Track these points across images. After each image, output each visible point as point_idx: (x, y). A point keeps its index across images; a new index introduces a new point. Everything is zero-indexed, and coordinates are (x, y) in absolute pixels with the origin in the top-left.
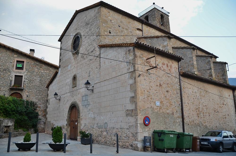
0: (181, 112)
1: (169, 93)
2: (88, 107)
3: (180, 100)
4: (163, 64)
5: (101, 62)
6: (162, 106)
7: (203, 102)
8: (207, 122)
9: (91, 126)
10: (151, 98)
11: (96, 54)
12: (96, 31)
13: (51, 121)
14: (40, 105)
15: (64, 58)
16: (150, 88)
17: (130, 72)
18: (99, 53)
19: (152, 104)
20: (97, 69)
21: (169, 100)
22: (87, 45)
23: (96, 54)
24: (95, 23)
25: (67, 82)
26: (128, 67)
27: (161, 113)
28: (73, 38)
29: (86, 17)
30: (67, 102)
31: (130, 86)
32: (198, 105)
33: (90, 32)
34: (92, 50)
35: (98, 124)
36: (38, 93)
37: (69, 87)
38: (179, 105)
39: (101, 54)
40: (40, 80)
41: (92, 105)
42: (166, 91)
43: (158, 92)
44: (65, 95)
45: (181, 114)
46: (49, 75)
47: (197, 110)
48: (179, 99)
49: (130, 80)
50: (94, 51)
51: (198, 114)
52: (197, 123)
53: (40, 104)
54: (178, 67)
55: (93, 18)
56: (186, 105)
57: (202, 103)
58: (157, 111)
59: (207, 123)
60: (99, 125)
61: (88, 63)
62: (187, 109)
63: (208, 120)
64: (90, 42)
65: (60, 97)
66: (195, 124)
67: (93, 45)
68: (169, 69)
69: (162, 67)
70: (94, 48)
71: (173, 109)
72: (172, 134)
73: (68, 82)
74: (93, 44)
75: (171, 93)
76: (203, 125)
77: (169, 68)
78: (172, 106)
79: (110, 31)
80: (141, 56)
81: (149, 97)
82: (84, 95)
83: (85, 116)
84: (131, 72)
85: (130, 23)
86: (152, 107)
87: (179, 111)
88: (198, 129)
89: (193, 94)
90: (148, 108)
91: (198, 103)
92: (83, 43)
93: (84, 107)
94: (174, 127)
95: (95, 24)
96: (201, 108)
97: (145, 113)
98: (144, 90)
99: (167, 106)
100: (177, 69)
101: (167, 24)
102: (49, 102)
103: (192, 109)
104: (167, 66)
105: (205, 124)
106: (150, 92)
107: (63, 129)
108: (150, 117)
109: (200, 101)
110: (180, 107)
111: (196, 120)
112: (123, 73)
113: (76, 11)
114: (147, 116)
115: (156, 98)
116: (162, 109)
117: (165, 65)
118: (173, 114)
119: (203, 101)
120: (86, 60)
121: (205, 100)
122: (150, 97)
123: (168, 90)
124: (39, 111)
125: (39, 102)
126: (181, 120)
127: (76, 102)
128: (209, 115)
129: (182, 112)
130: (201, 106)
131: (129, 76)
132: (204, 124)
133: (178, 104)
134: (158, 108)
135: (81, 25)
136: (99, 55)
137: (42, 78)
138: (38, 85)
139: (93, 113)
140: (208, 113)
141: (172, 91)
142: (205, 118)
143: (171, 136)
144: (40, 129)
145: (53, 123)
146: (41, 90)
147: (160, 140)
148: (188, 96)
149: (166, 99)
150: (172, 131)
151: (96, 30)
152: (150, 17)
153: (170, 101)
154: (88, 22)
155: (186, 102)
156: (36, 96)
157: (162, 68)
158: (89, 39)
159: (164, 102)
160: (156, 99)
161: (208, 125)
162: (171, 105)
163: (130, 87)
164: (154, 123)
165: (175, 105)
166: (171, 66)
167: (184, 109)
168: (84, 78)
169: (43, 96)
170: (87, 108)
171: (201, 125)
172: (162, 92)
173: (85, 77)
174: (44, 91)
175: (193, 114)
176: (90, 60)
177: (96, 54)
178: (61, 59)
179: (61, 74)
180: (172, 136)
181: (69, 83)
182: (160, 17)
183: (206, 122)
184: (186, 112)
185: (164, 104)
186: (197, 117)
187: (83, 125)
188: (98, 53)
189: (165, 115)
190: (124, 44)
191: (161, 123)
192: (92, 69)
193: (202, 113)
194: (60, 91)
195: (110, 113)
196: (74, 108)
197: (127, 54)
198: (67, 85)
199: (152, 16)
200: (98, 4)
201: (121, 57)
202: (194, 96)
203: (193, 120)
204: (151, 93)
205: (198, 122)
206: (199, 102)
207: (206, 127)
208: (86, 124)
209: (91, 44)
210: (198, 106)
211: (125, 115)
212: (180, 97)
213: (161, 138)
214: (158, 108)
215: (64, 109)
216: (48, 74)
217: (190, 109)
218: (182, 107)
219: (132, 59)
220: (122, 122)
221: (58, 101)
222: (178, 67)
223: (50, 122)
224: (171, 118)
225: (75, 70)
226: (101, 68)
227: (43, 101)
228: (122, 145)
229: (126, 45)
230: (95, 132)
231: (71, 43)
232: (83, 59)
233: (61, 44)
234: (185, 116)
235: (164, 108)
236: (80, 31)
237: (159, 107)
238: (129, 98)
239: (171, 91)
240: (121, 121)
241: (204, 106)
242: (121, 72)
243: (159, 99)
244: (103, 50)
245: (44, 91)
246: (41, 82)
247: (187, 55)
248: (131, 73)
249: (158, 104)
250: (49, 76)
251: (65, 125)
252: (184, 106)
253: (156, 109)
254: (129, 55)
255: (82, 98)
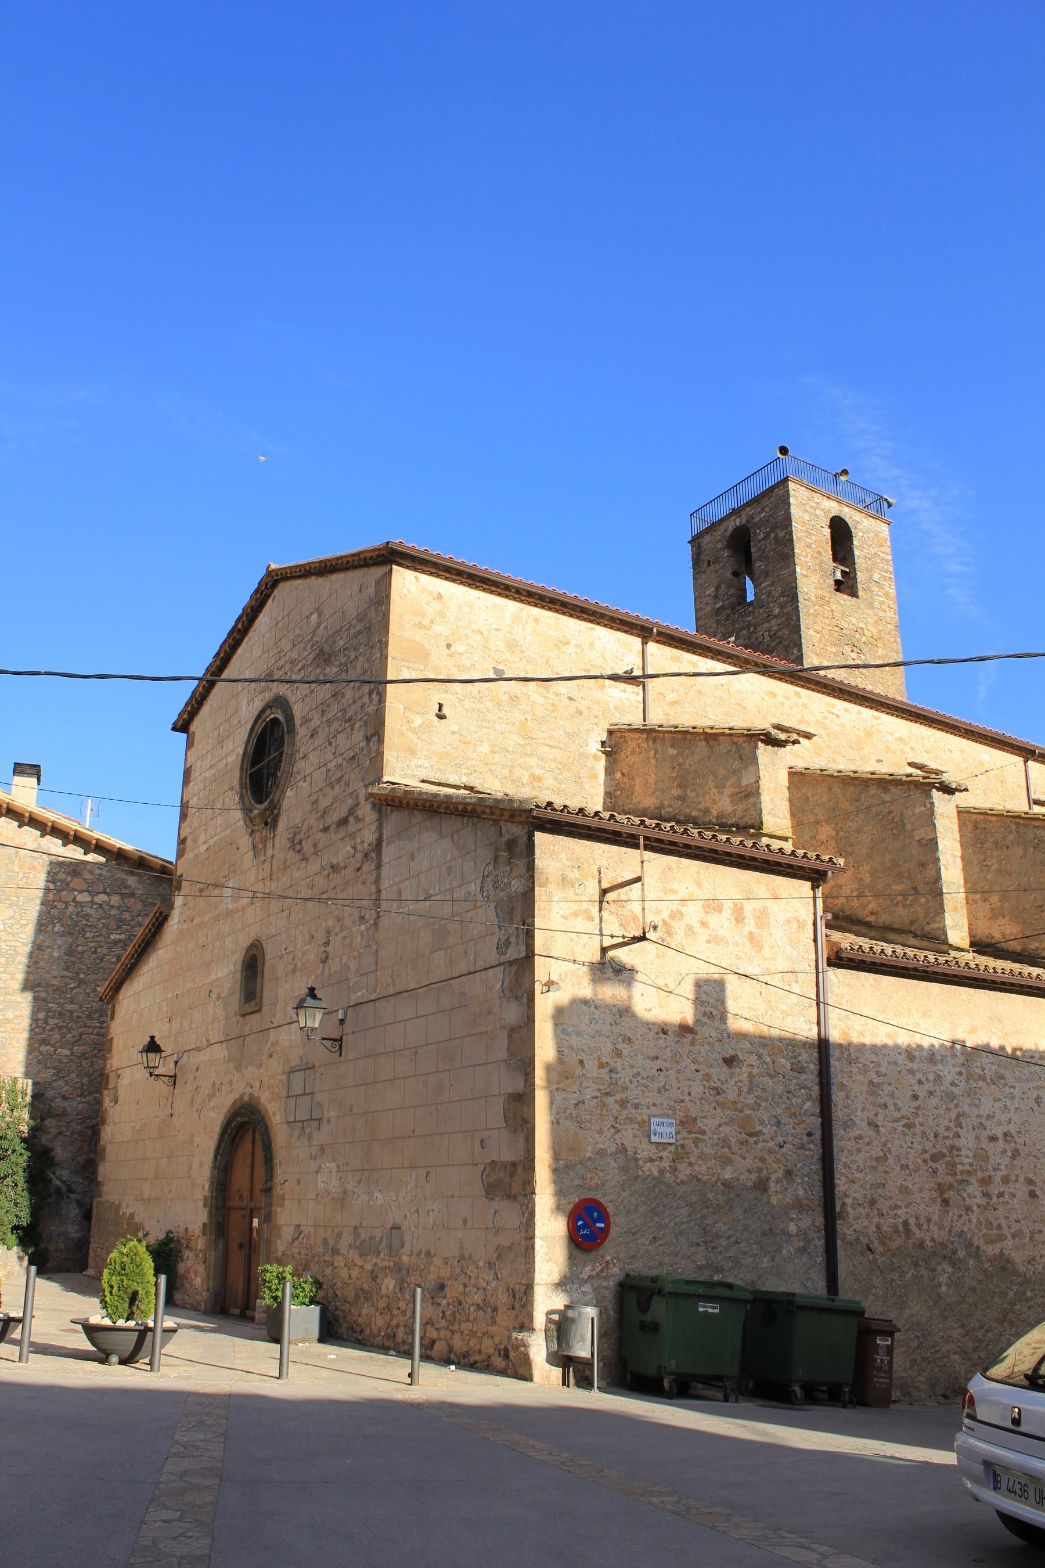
0: (817, 1178)
1: (744, 1069)
2: (315, 1135)
3: (812, 1107)
4: (712, 904)
5: (382, 887)
6: (689, 1143)
7: (989, 1117)
8: (1014, 1236)
9: (325, 1241)
10: (623, 1103)
11: (359, 840)
12: (362, 707)
13: (124, 1205)
14: (66, 1104)
15: (202, 839)
16: (620, 1046)
17: (511, 963)
18: (376, 836)
19: (628, 1136)
20: (363, 927)
21: (736, 1109)
22: (319, 776)
23: (359, 840)
24: (361, 659)
25: (213, 977)
26: (501, 935)
27: (683, 1182)
28: (252, 729)
29: (320, 615)
30: (210, 1097)
31: (510, 1037)
32: (943, 1133)
33: (335, 708)
34: (343, 815)
35: (360, 1231)
36: (52, 1030)
37: (225, 1009)
38: (809, 1135)
39: (384, 843)
40: (70, 952)
41: (333, 1123)
42: (719, 1057)
43: (667, 1065)
44: (202, 1057)
45: (818, 1190)
46: (121, 920)
47: (941, 1166)
48: (809, 1104)
49: (508, 1002)
50: (351, 819)
51: (941, 1188)
52: (933, 1240)
53: (64, 1098)
54: (812, 917)
55: (353, 631)
56: (860, 1137)
57: (975, 1121)
58: (656, 1173)
59: (1009, 1243)
60: (364, 1235)
61: (321, 882)
62: (860, 1159)
63: (1018, 1221)
64: (334, 763)
65: (176, 1062)
66: (921, 1244)
67: (347, 784)
68: (751, 934)
69: (703, 924)
70: (350, 802)
71: (762, 1160)
72: (710, 1299)
73: (218, 979)
74: (346, 777)
75: (755, 1071)
76: (977, 1253)
77: (751, 925)
78: (760, 1145)
79: (440, 710)
80: (574, 874)
81: (607, 1094)
82: (295, 1062)
83: (299, 1182)
84: (515, 961)
85: (568, 643)
86: (623, 1150)
87: (806, 1170)
88: (943, 1279)
89: (911, 1072)
90: (601, 1153)
91: (946, 1123)
92: (303, 764)
93: (296, 1133)
94: (766, 1262)
95: (359, 665)
96: (971, 1154)
97: (577, 1182)
98: (582, 1056)
99: (725, 1143)
100: (801, 926)
101: (876, 577)
102: (116, 1088)
103: (898, 1158)
104: (739, 918)
105: (999, 1245)
106: (619, 1069)
107: (187, 1253)
108: (611, 1202)
109: (966, 1108)
110: (815, 1149)
111: (929, 1220)
112: (481, 964)
113: (269, 573)
114: (601, 1204)
115: (651, 1100)
116: (693, 1159)
117: (721, 912)
118: (762, 1186)
119: (986, 1108)
120: (314, 867)
121: (999, 1104)
122: (618, 1097)
123: (731, 1052)
124: (61, 1138)
125: (61, 1082)
126: (820, 1221)
127: (258, 1099)
128: (1033, 1195)
129: (824, 1176)
130: (967, 1141)
131: (506, 983)
132: (992, 1250)
133: (801, 1130)
134: (664, 1154)
135: (294, 655)
136: (376, 845)
137: (81, 941)
138: (54, 982)
139: (338, 1166)
140: (1021, 1179)
141: (760, 1057)
142: (995, 1209)
143: (701, 1309)
144: (56, 1250)
145: (132, 1215)
146: (72, 1013)
147: (643, 1327)
148: (871, 1083)
149: (722, 1105)
150: (712, 1285)
151: (366, 699)
152: (762, 536)
153: (747, 1112)
154: (327, 649)
155: (860, 1118)
156: (43, 1048)
157: (703, 930)
158: (330, 744)
159: (708, 1124)
160: (654, 1105)
161: (1017, 1257)
162: (752, 1135)
163: (509, 1045)
164: (634, 1234)
165: (780, 1139)
166: (762, 919)
167: (841, 1160)
168: (299, 965)
169: (82, 1048)
170: (310, 1137)
171: (961, 1254)
172: (694, 1067)
173: (303, 964)
174: (89, 1017)
175: (905, 1190)
176: (332, 867)
177: (362, 842)
178: (185, 839)
179: (185, 926)
180: (710, 1310)
181: (227, 985)
182: (827, 532)
183: (1001, 1238)
184: (858, 1175)
185: (703, 1132)
186: (936, 1210)
187: (287, 1233)
188: (369, 836)
189: (710, 1196)
190: (488, 811)
191: (682, 1239)
192: (339, 921)
193: (973, 1180)
194: (175, 1026)
195: (414, 1174)
196: (244, 1131)
197: (501, 860)
198: (214, 995)
199: (773, 530)
200: (378, 556)
201: (474, 877)
202: (920, 1082)
203: (906, 1223)
204: (624, 1077)
205: (940, 1235)
206: (959, 1115)
207: (1003, 1269)
208: (302, 1228)
209: (339, 780)
210: (948, 1142)
211: (479, 1189)
212: (816, 1088)
213: (648, 1318)
214: (664, 1154)
215: (193, 1135)
216: (114, 912)
217: (881, 1160)
218: (824, 1147)
219: (522, 894)
220: (469, 1225)
221: (162, 1087)
222: (815, 914)
223: (119, 1207)
224: (745, 1212)
225: (258, 918)
226: (384, 922)
227: (85, 1080)
228: (465, 1349)
229: (493, 814)
230: (344, 1273)
231: (241, 753)
232: (298, 857)
233: (190, 744)
234: (849, 1201)
235: (702, 1156)
236: (289, 693)
237: (672, 1148)
238: (502, 1099)
239: (753, 1059)
240: (465, 1221)
241: (993, 1139)
242: (472, 958)
243: (673, 1104)
244: (394, 820)
245: (89, 1017)
246: (74, 962)
247: (909, 826)
248: (514, 968)
249: (665, 1130)
250: (119, 927)
251: (196, 1228)
252: (842, 1140)
253: (652, 1160)
254: (508, 869)
255: (285, 1077)
